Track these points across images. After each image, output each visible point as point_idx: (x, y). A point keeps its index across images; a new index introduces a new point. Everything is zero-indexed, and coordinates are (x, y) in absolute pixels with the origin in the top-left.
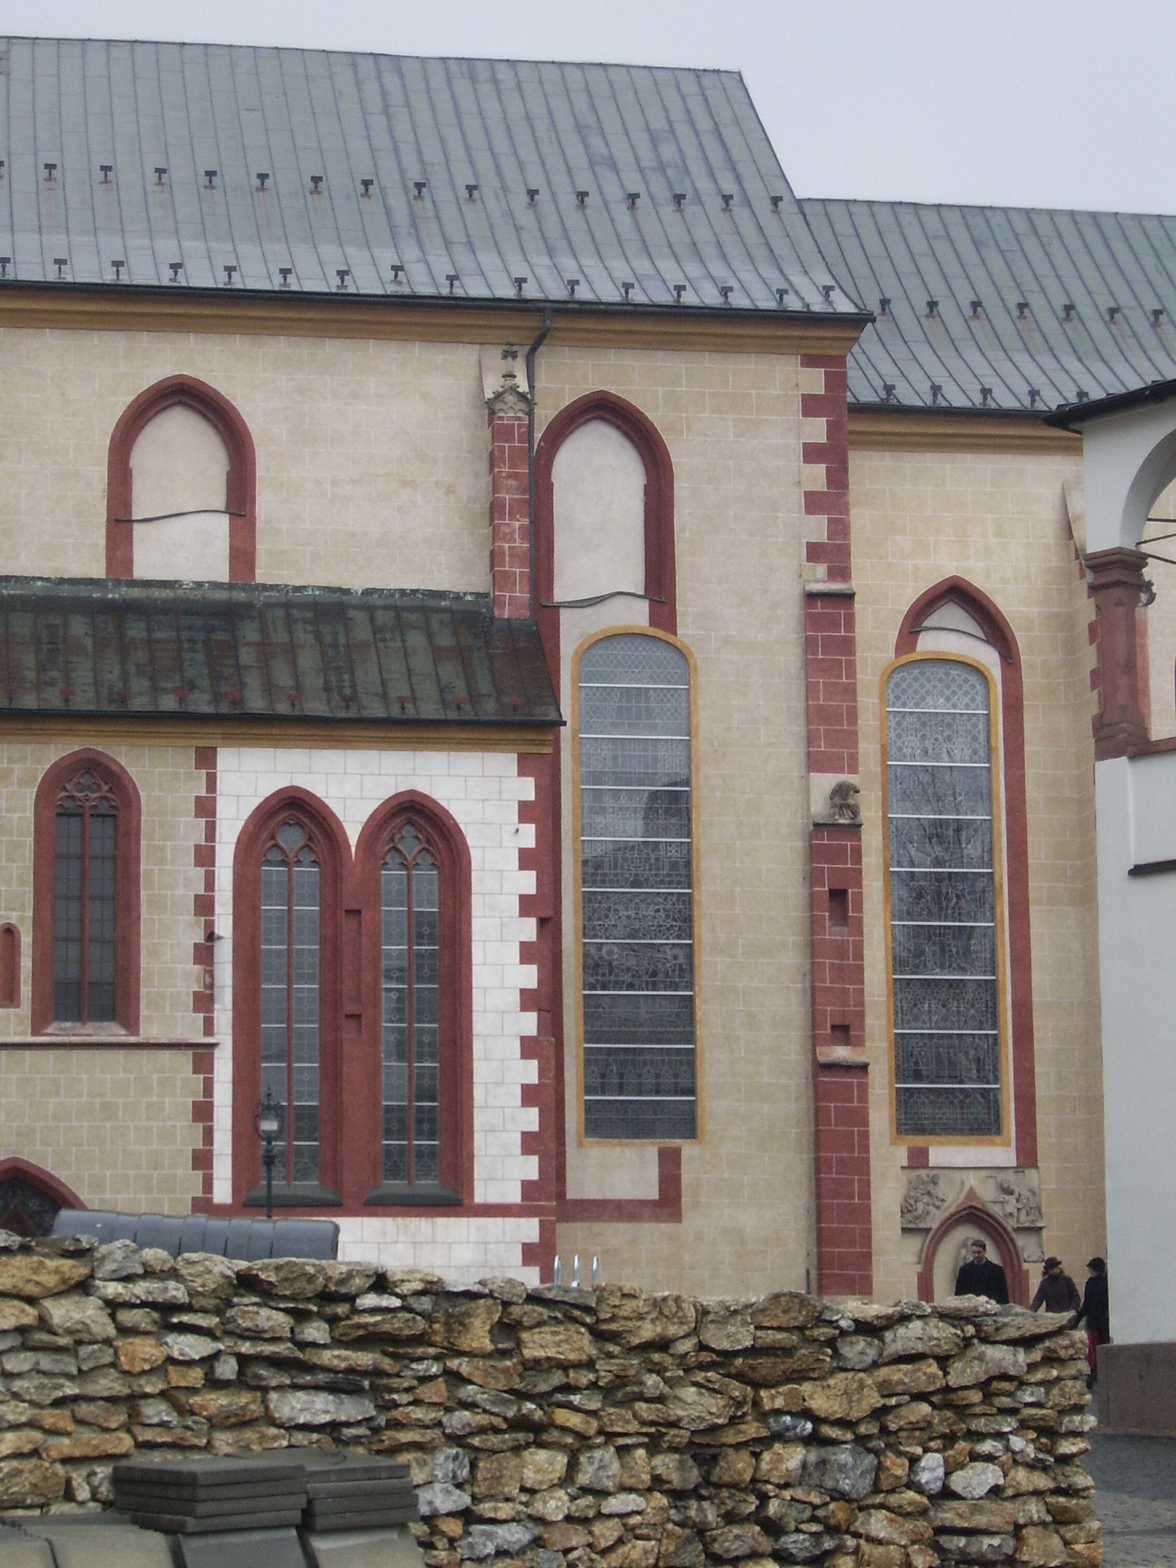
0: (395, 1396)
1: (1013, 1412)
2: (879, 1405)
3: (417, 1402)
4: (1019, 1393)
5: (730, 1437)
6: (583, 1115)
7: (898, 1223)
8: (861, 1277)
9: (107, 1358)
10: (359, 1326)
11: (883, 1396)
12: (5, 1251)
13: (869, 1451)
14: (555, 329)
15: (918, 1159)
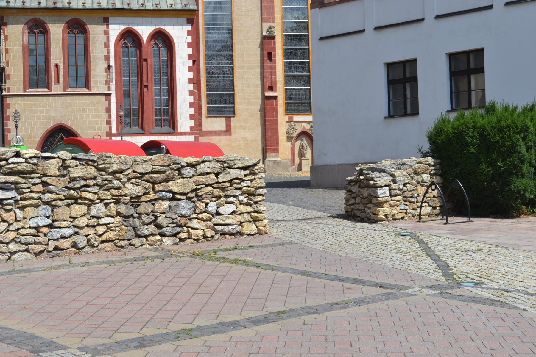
0: (23, 190)
1: (240, 189)
2: (195, 188)
3: (31, 192)
4: (242, 183)
5: (144, 199)
6: (204, 31)
7: (286, 135)
8: (276, 149)
9: (156, 186)
10: (11, 168)
11: (196, 185)
13: (192, 202)
15: (290, 120)
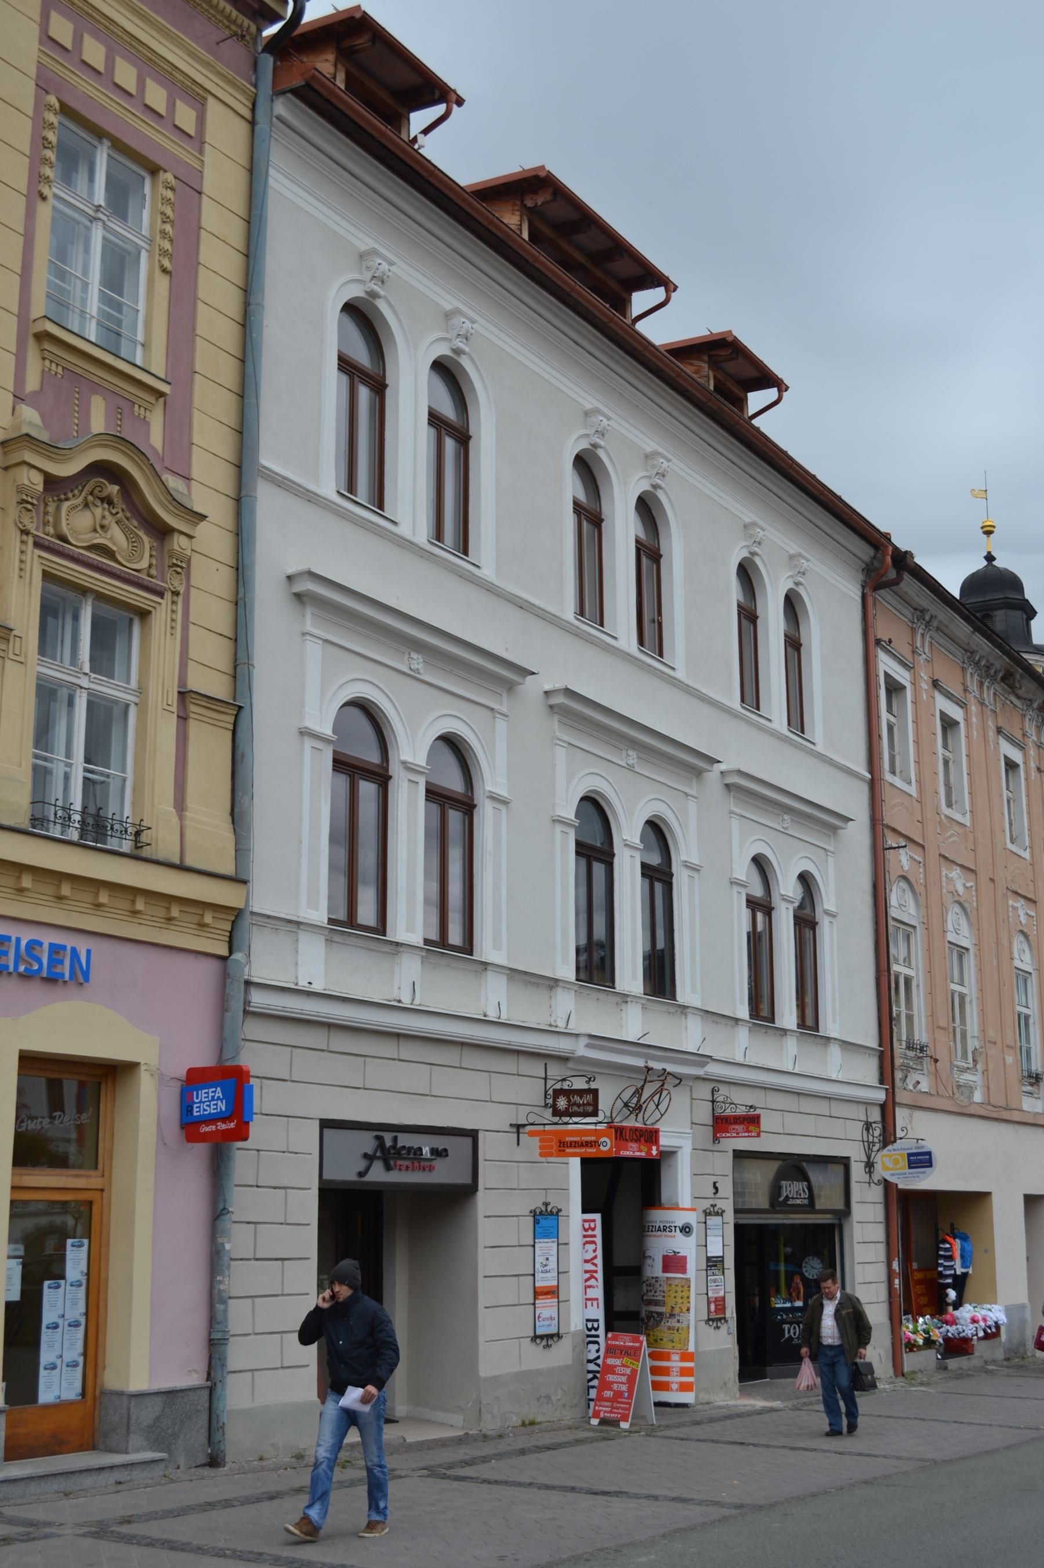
12: (6, 1541)
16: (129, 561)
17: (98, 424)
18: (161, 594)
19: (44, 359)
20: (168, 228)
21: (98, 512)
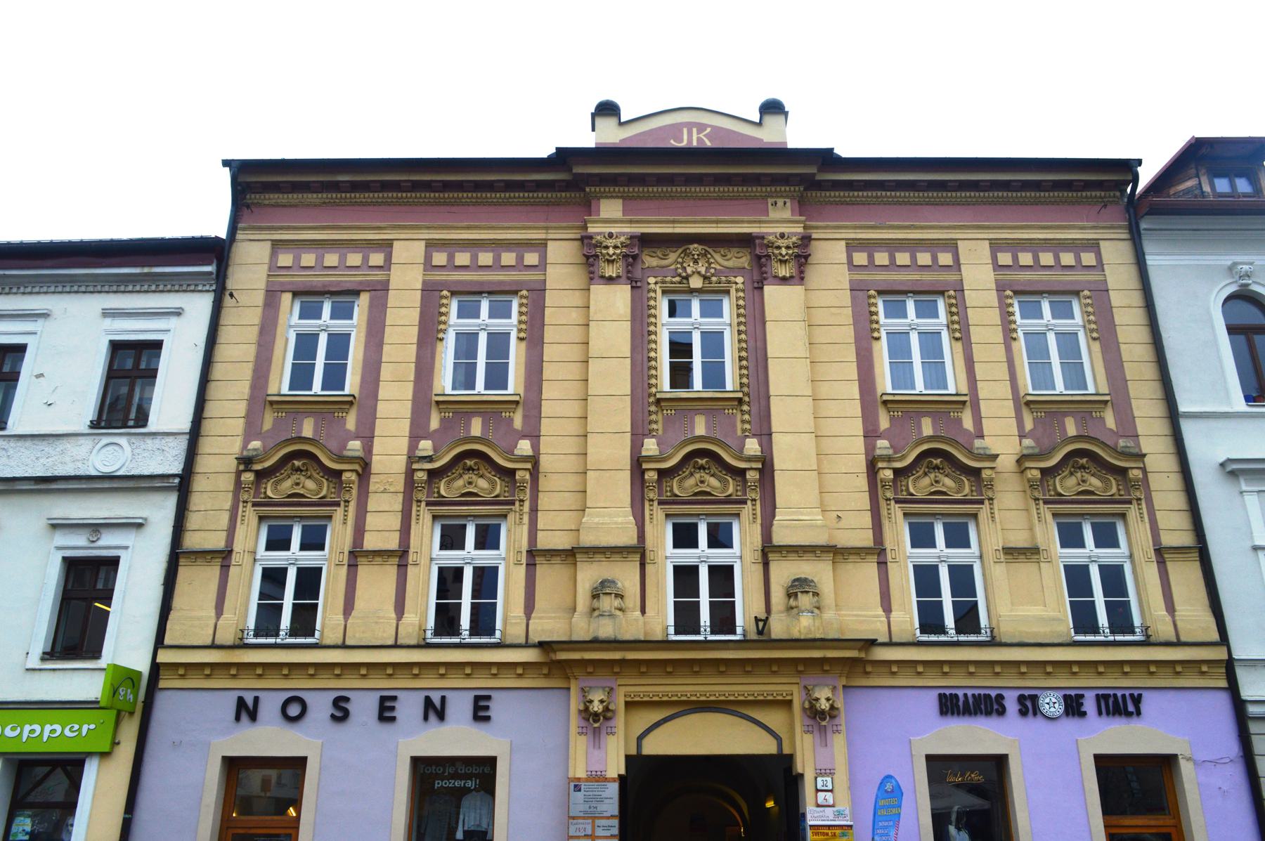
14: (996, 526)
16: (1103, 492)
17: (1071, 430)
18: (1130, 502)
19: (1033, 413)
20: (1092, 317)
21: (1079, 475)
